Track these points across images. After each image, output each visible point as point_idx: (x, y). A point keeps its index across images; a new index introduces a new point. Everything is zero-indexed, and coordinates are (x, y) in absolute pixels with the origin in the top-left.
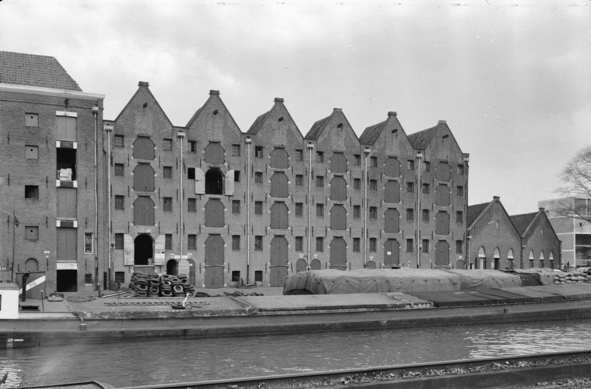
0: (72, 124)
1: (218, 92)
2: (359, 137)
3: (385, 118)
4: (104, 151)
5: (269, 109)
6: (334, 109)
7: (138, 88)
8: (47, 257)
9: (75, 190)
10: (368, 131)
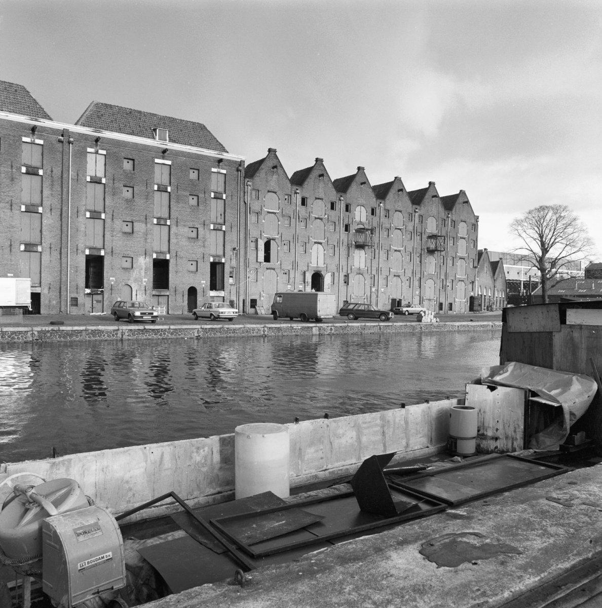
0: (166, 171)
1: (322, 159)
3: (264, 154)
8: (204, 285)
9: (40, 215)
10: (296, 174)
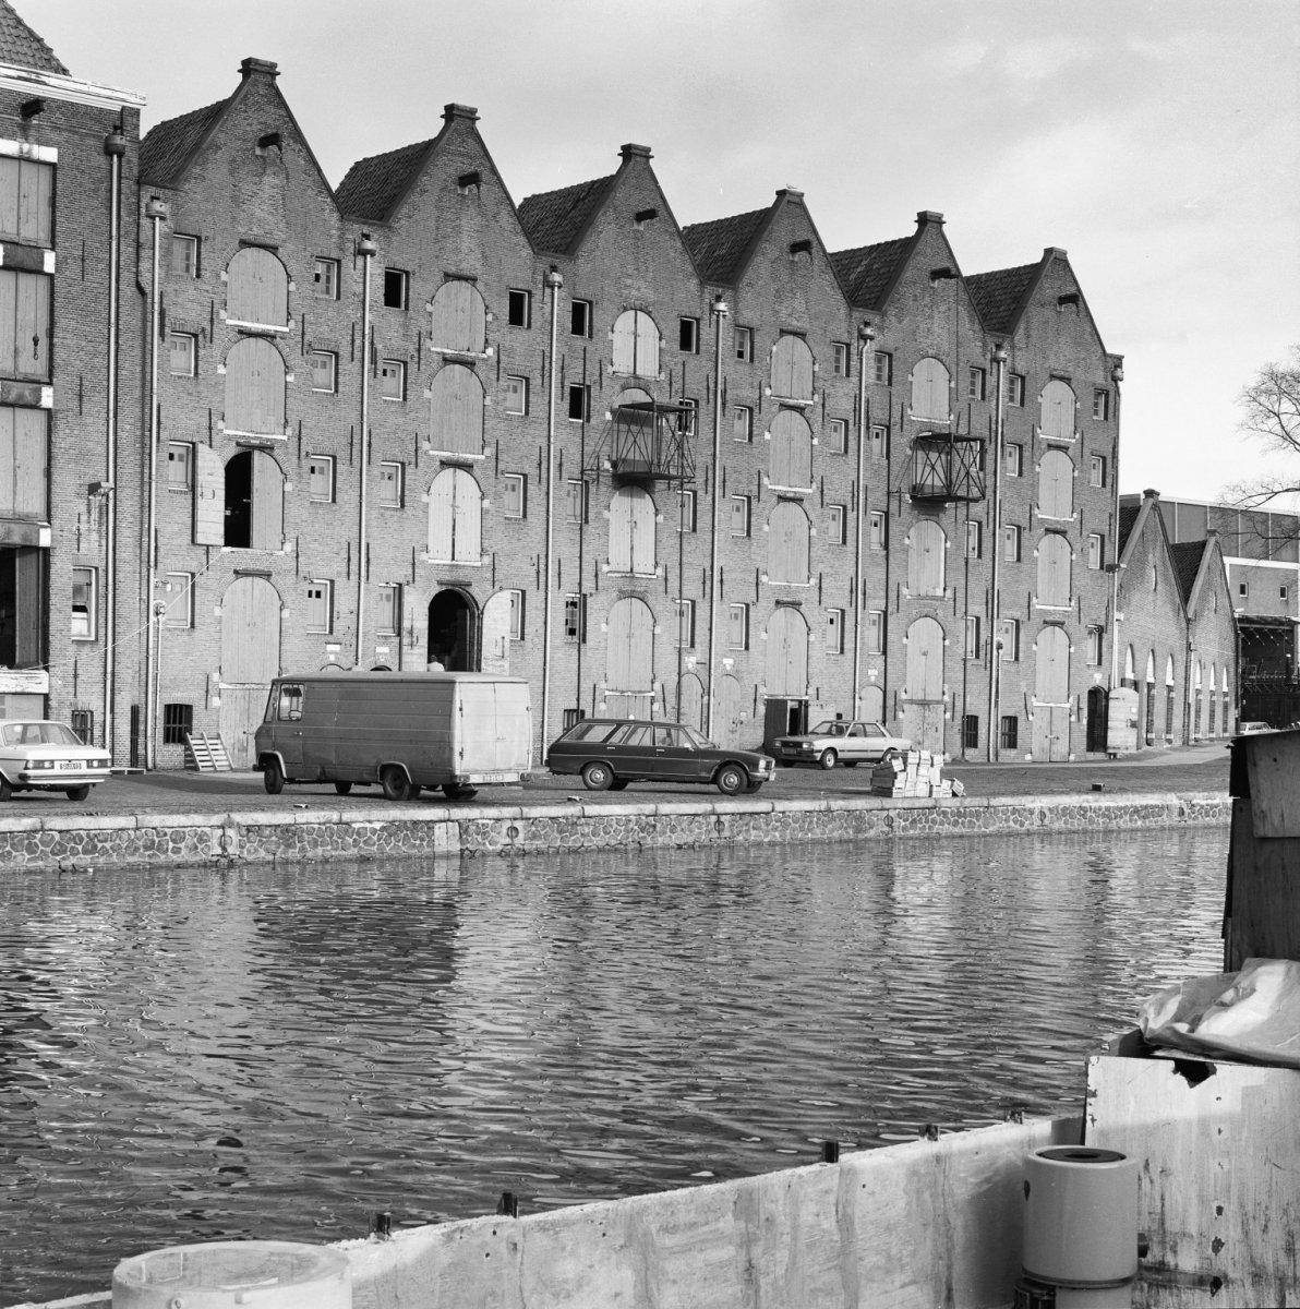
1: (473, 111)
2: (335, 186)
3: (226, 84)
4: (138, 286)
5: (228, 94)
6: (778, 193)
7: (775, 197)
